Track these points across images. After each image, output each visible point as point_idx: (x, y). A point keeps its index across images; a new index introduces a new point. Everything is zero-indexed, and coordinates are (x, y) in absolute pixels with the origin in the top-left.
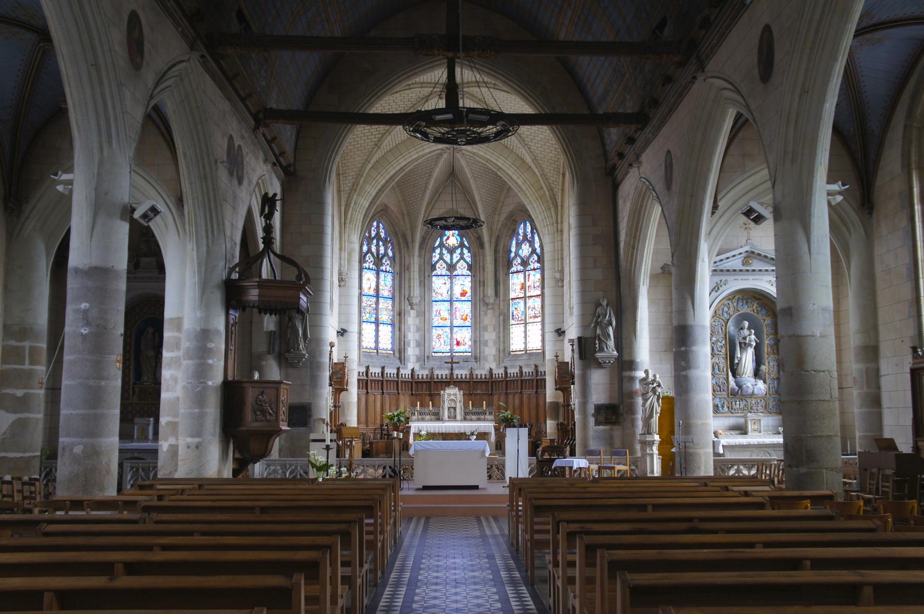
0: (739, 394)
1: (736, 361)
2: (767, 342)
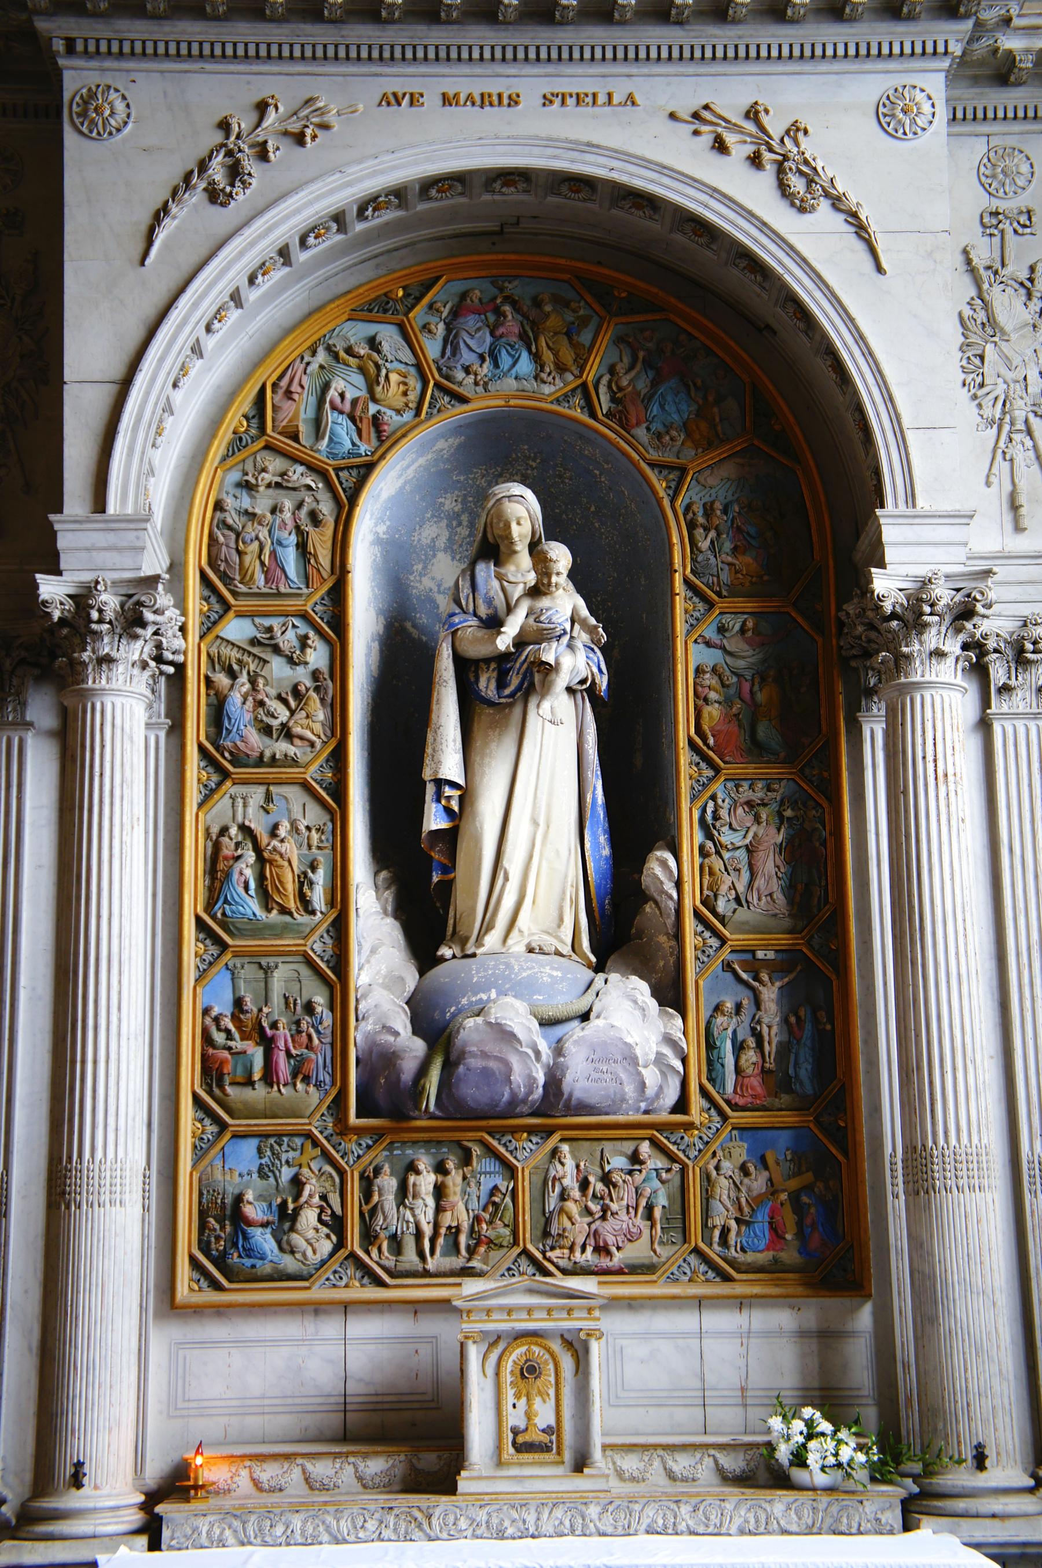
1: (435, 820)
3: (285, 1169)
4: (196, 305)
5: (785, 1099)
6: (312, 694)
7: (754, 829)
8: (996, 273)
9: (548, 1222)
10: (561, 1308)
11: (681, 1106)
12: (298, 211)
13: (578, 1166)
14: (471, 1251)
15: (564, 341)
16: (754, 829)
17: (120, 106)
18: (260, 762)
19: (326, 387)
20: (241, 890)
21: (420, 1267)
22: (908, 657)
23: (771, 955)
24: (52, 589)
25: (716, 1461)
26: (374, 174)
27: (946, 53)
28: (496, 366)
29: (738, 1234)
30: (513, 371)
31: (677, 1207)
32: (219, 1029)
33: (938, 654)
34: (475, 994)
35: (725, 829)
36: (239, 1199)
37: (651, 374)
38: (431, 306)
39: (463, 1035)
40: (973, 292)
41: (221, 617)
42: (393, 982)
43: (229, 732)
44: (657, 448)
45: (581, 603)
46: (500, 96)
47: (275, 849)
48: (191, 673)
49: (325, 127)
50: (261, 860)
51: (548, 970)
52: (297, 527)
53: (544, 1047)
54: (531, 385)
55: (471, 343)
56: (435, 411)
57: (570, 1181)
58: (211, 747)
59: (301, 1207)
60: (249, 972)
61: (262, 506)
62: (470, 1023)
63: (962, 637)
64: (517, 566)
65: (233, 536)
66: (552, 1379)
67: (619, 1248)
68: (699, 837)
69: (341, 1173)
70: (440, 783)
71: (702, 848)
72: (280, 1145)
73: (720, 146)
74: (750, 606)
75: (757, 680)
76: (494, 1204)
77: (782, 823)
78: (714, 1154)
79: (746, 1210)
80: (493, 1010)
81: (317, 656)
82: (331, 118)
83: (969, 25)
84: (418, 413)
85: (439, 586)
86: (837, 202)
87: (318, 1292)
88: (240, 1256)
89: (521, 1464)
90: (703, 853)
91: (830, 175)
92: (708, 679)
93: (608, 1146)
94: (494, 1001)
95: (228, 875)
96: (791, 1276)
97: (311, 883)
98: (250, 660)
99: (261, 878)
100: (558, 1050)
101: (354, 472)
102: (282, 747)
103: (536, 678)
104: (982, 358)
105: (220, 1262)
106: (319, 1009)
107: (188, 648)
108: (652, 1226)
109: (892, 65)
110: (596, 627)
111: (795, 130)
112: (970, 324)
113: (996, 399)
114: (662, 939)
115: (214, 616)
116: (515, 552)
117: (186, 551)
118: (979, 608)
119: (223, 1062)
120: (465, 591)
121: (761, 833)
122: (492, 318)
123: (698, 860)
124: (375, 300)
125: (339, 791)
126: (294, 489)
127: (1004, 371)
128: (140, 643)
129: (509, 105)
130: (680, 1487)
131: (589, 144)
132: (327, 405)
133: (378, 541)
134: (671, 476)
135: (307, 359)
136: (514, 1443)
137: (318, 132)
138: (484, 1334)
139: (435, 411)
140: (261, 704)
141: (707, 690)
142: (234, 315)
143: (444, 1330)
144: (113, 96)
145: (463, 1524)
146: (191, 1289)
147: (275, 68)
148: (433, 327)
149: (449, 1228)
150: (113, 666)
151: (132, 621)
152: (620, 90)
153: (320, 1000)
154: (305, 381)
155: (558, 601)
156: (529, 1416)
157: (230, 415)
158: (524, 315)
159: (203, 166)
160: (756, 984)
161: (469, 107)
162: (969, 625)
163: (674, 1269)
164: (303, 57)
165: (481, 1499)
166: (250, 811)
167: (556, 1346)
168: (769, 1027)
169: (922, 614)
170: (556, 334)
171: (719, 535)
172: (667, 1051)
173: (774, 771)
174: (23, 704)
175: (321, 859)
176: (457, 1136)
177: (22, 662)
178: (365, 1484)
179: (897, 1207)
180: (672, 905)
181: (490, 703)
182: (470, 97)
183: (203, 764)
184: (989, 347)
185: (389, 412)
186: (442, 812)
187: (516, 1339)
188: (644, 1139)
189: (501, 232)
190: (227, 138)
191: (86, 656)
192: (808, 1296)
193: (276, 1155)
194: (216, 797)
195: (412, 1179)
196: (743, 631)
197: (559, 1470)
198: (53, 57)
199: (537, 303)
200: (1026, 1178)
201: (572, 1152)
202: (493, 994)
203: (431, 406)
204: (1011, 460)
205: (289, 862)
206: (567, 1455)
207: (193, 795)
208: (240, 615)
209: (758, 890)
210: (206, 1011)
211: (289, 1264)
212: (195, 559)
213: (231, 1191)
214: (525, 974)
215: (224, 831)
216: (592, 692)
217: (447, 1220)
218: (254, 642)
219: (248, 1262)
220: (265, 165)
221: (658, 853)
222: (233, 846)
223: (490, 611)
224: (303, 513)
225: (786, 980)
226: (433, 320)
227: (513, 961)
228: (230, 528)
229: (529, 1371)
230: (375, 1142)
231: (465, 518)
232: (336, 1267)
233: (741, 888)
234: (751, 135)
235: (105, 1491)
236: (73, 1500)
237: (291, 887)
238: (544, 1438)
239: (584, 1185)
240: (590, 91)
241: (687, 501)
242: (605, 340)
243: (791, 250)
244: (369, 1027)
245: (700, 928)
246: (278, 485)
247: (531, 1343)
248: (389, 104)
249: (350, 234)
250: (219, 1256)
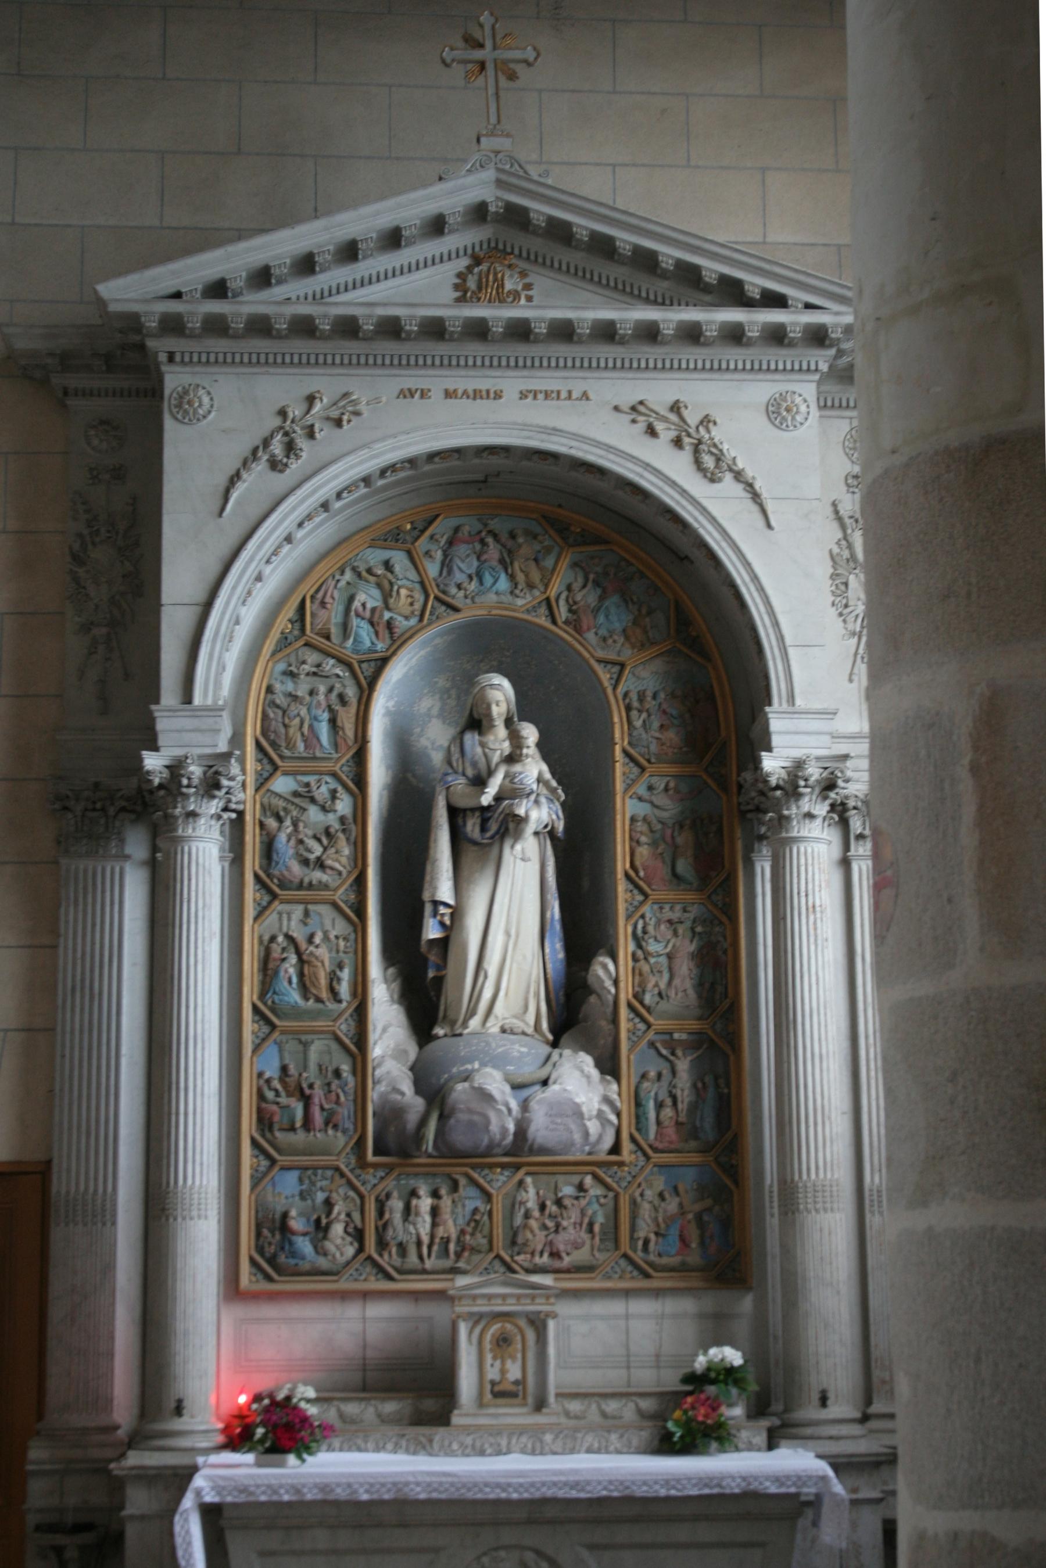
0: (427, 1142)
1: (432, 931)
2: (634, 805)
4: (259, 547)
5: (693, 1144)
6: (341, 835)
7: (673, 941)
9: (515, 1234)
10: (526, 1296)
11: (616, 1149)
12: (336, 477)
13: (538, 1193)
14: (458, 1255)
15: (532, 564)
16: (673, 941)
17: (206, 400)
18: (300, 886)
19: (351, 599)
20: (286, 983)
21: (420, 1267)
22: (788, 818)
23: (684, 1036)
24: (153, 762)
25: (637, 1405)
26: (394, 449)
27: (817, 370)
28: (481, 583)
29: (656, 1243)
30: (494, 588)
31: (612, 1224)
32: (270, 1089)
33: (810, 816)
34: (463, 1064)
35: (651, 941)
36: (285, 1215)
37: (599, 591)
38: (432, 537)
39: (454, 1096)
40: (840, 535)
41: (271, 775)
42: (399, 1054)
43: (277, 863)
44: (603, 649)
45: (545, 768)
46: (488, 392)
47: (311, 953)
48: (248, 818)
49: (357, 414)
50: (301, 961)
51: (518, 1048)
52: (329, 706)
53: (514, 1105)
54: (507, 599)
55: (462, 565)
56: (434, 618)
57: (532, 1204)
58: (264, 875)
60: (292, 1046)
61: (302, 692)
62: (460, 1087)
63: (828, 802)
64: (496, 735)
65: (280, 713)
66: (519, 1346)
68: (631, 947)
69: (362, 1197)
70: (436, 903)
71: (634, 955)
72: (316, 1175)
73: (651, 432)
74: (673, 770)
75: (677, 827)
76: (476, 1221)
77: (694, 937)
78: (639, 1185)
79: (663, 1226)
80: (476, 1078)
81: (344, 806)
82: (362, 407)
83: (833, 352)
84: (421, 619)
85: (433, 744)
86: (738, 475)
87: (344, 1284)
88: (287, 1257)
89: (497, 1406)
90: (635, 959)
91: (733, 455)
92: (640, 826)
93: (561, 1179)
94: (478, 1070)
95: (276, 972)
96: (693, 1274)
97: (339, 980)
98: (293, 807)
99: (301, 975)
100: (525, 1106)
101: (373, 664)
102: (317, 875)
103: (510, 826)
104: (846, 584)
105: (272, 1261)
106: (345, 1075)
107: (246, 798)
108: (593, 1238)
109: (777, 377)
110: (556, 789)
111: (707, 421)
112: (837, 559)
113: (857, 616)
114: (603, 1023)
115: (266, 775)
116: (494, 726)
117: (244, 724)
118: (840, 783)
119: (272, 1114)
120: (456, 756)
121: (678, 944)
122: (478, 546)
123: (630, 963)
124: (389, 532)
125: (360, 910)
126: (327, 677)
128: (216, 801)
129: (495, 398)
130: (611, 1422)
131: (555, 429)
132: (353, 613)
133: (388, 713)
134: (614, 670)
135: (337, 577)
136: (492, 1392)
137: (352, 418)
138: (471, 1314)
139: (434, 618)
140: (301, 842)
141: (638, 835)
142: (287, 548)
143: (438, 1313)
144: (201, 392)
145: (455, 1446)
146: (250, 1281)
147: (321, 371)
148: (433, 553)
149: (442, 1238)
150: (197, 819)
151: (211, 785)
153: (345, 1068)
154: (336, 594)
155: (528, 767)
156: (503, 1372)
157: (279, 621)
158: (504, 546)
159: (266, 443)
160: (672, 1058)
161: (464, 400)
162: (832, 795)
163: (608, 1269)
164: (342, 364)
165: (467, 1429)
166: (293, 923)
167: (522, 1323)
168: (682, 1090)
169: (798, 787)
170: (527, 559)
171: (649, 715)
172: (606, 1108)
173: (690, 897)
174: (122, 841)
175: (347, 961)
176: (448, 1170)
177: (123, 809)
178: (384, 1420)
179: (773, 1222)
180: (610, 998)
181: (475, 843)
182: (465, 392)
183: (257, 887)
185: (400, 618)
186: (437, 926)
187: (494, 1318)
188: (587, 1173)
189: (485, 481)
190: (285, 421)
191: (178, 811)
192: (705, 1289)
193: (313, 1183)
194: (267, 913)
195: (414, 1202)
196: (666, 789)
197: (524, 1410)
198: (157, 365)
199: (513, 536)
200: (867, 1202)
201: (534, 1183)
202: (476, 1065)
203: (431, 614)
205: (322, 962)
206: (530, 1400)
207: (250, 912)
208: (286, 773)
209: (676, 988)
210: (260, 1075)
211: (323, 1263)
212: (251, 731)
213: (280, 1210)
214: (500, 1050)
215: (273, 939)
216: (552, 834)
217: (440, 1232)
218: (296, 794)
219: (292, 1261)
220: (313, 442)
221: (601, 959)
222: (279, 950)
223: (475, 772)
224: (333, 696)
225: (695, 1055)
226: (433, 547)
227: (491, 1039)
228: (278, 707)
229: (503, 1342)
230: (387, 1174)
231: (453, 692)
232: (357, 1266)
233: (663, 985)
234: (674, 424)
235: (199, 1419)
236: (177, 1424)
237: (323, 982)
238: (513, 1388)
239: (543, 1207)
240: (555, 388)
241: (625, 689)
242: (564, 564)
243: (704, 511)
244: (383, 1089)
245: (632, 1016)
246: (315, 674)
247: (504, 1321)
248: (405, 397)
249: (373, 488)
250: (271, 1258)
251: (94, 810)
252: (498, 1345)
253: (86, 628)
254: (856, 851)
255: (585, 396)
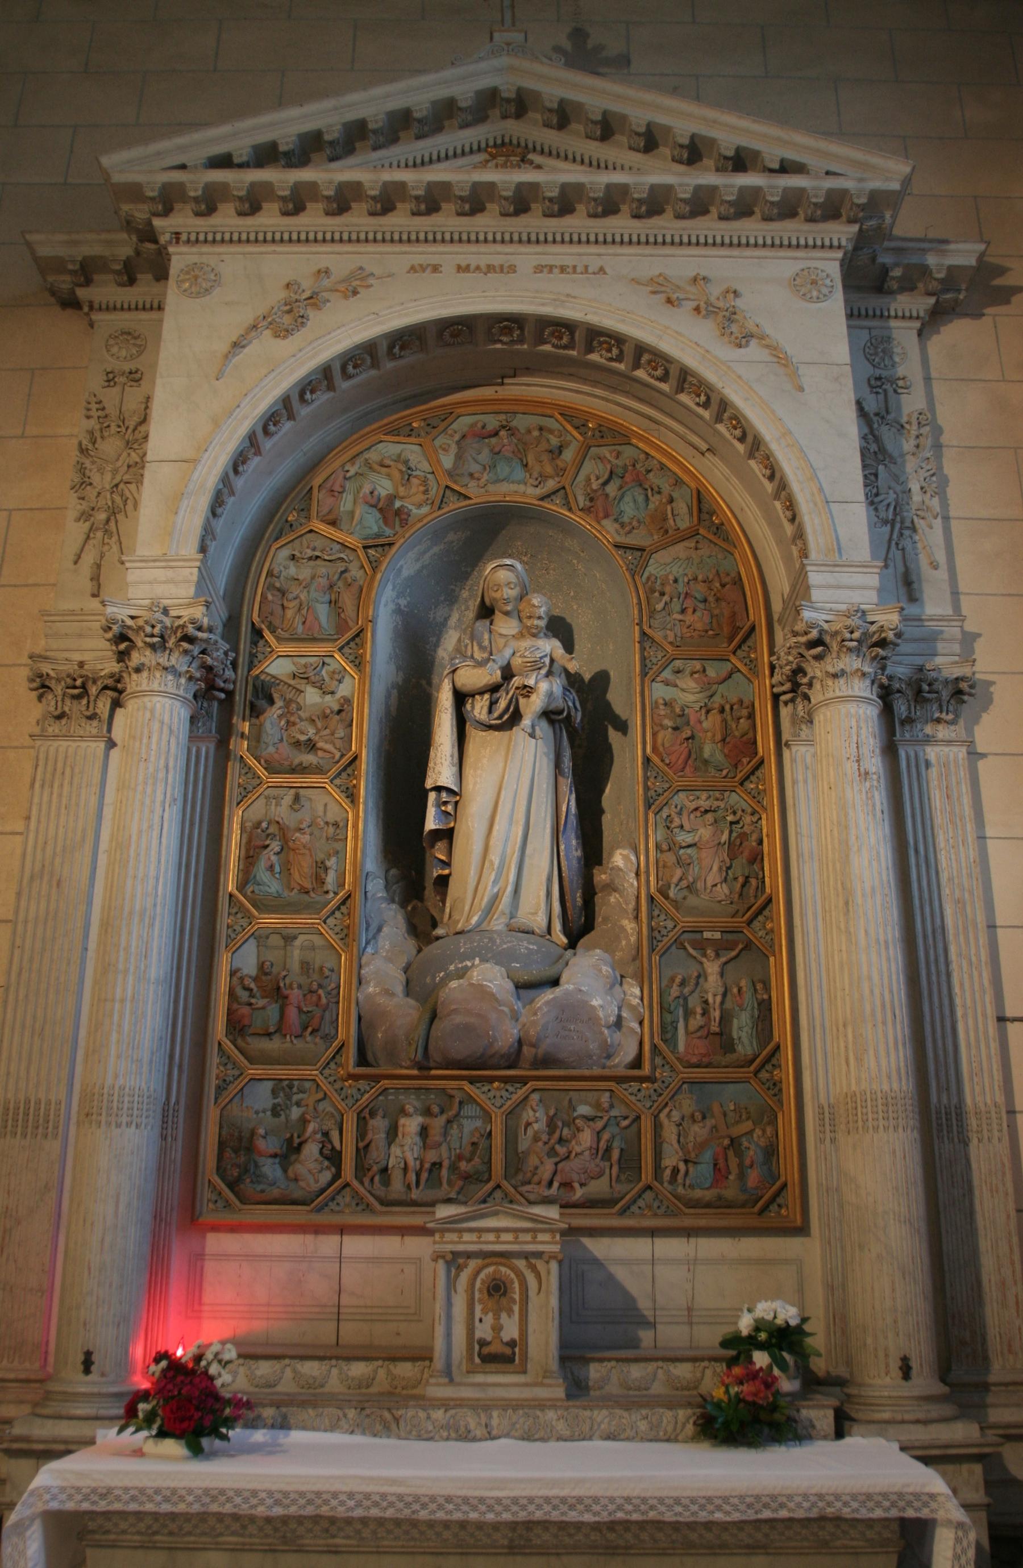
3: (295, 1109)
8: (883, 418)
23: (718, 935)
59: (305, 1141)
67: (582, 1185)
92: (662, 711)
104: (876, 475)
113: (889, 505)
127: (893, 484)
136: (479, 1355)
152: (594, 264)
156: (497, 1328)
182: (478, 268)
184: (881, 468)
202: (477, 961)
204: (903, 549)
229: (497, 1289)
238: (508, 1351)
251: (75, 687)
252: (490, 1294)
253: (85, 516)
254: (902, 735)
255: (602, 270)
